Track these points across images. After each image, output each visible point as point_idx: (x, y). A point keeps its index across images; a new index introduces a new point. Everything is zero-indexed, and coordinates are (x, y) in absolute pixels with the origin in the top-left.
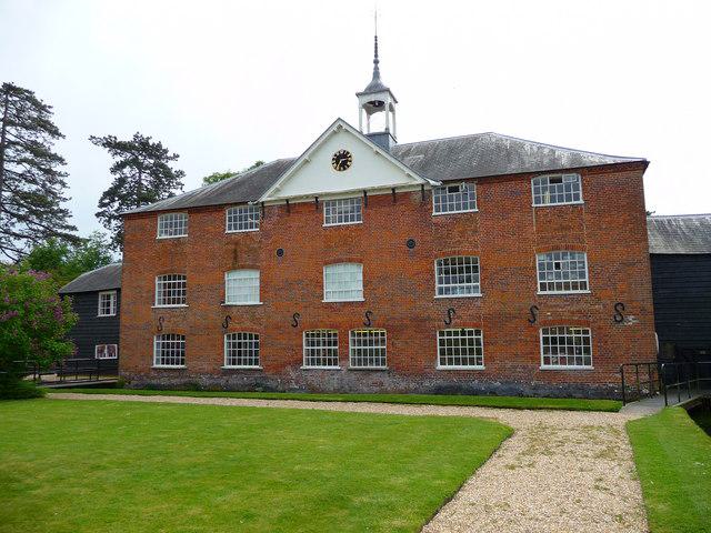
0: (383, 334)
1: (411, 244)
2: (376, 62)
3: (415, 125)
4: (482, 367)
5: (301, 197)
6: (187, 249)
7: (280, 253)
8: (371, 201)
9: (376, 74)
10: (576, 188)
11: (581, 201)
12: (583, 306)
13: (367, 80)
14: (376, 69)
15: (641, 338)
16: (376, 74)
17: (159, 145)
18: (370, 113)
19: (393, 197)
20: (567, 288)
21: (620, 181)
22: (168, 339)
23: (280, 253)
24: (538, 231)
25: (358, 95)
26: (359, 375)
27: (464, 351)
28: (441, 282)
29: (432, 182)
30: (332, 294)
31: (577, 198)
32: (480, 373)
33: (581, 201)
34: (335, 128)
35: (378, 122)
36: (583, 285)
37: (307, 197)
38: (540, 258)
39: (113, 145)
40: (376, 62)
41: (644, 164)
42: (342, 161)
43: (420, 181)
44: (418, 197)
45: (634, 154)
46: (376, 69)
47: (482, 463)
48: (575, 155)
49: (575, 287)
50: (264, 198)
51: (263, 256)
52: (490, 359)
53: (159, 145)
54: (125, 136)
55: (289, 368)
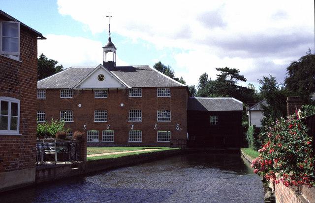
4: (141, 142)
6: (45, 103)
9: (110, 39)
10: (169, 92)
16: (110, 39)
17: (226, 68)
18: (107, 52)
21: (31, 36)
24: (159, 103)
27: (136, 137)
28: (130, 117)
31: (169, 95)
34: (99, 67)
35: (109, 57)
38: (158, 112)
42: (101, 78)
49: (167, 120)
53: (226, 68)
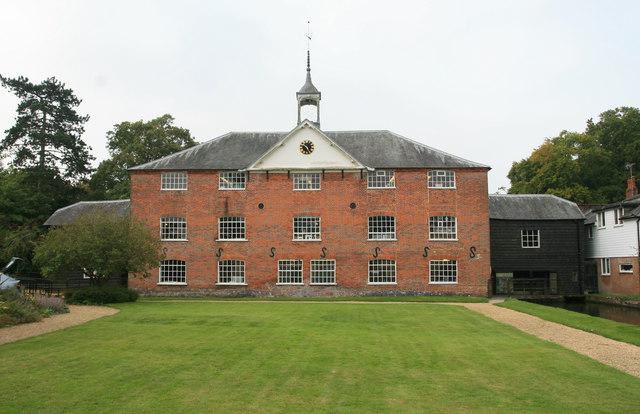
0: (525, 244)
1: (353, 206)
2: (309, 70)
3: (337, 116)
5: (278, 170)
7: (261, 206)
8: (325, 175)
11: (455, 187)
12: (454, 248)
13: (301, 84)
14: (309, 75)
15: (481, 264)
19: (343, 174)
20: (445, 237)
22: (175, 263)
23: (261, 206)
25: (298, 93)
26: (317, 288)
29: (369, 169)
30: (628, 250)
32: (394, 286)
33: (455, 187)
36: (454, 236)
37: (283, 170)
39: (20, 86)
40: (309, 70)
41: (489, 169)
43: (361, 167)
44: (358, 176)
45: (484, 163)
46: (309, 75)
47: (573, 220)
48: (448, 158)
50: (251, 168)
51: (247, 208)
52: (400, 278)
54: (36, 80)
55: (267, 284)
